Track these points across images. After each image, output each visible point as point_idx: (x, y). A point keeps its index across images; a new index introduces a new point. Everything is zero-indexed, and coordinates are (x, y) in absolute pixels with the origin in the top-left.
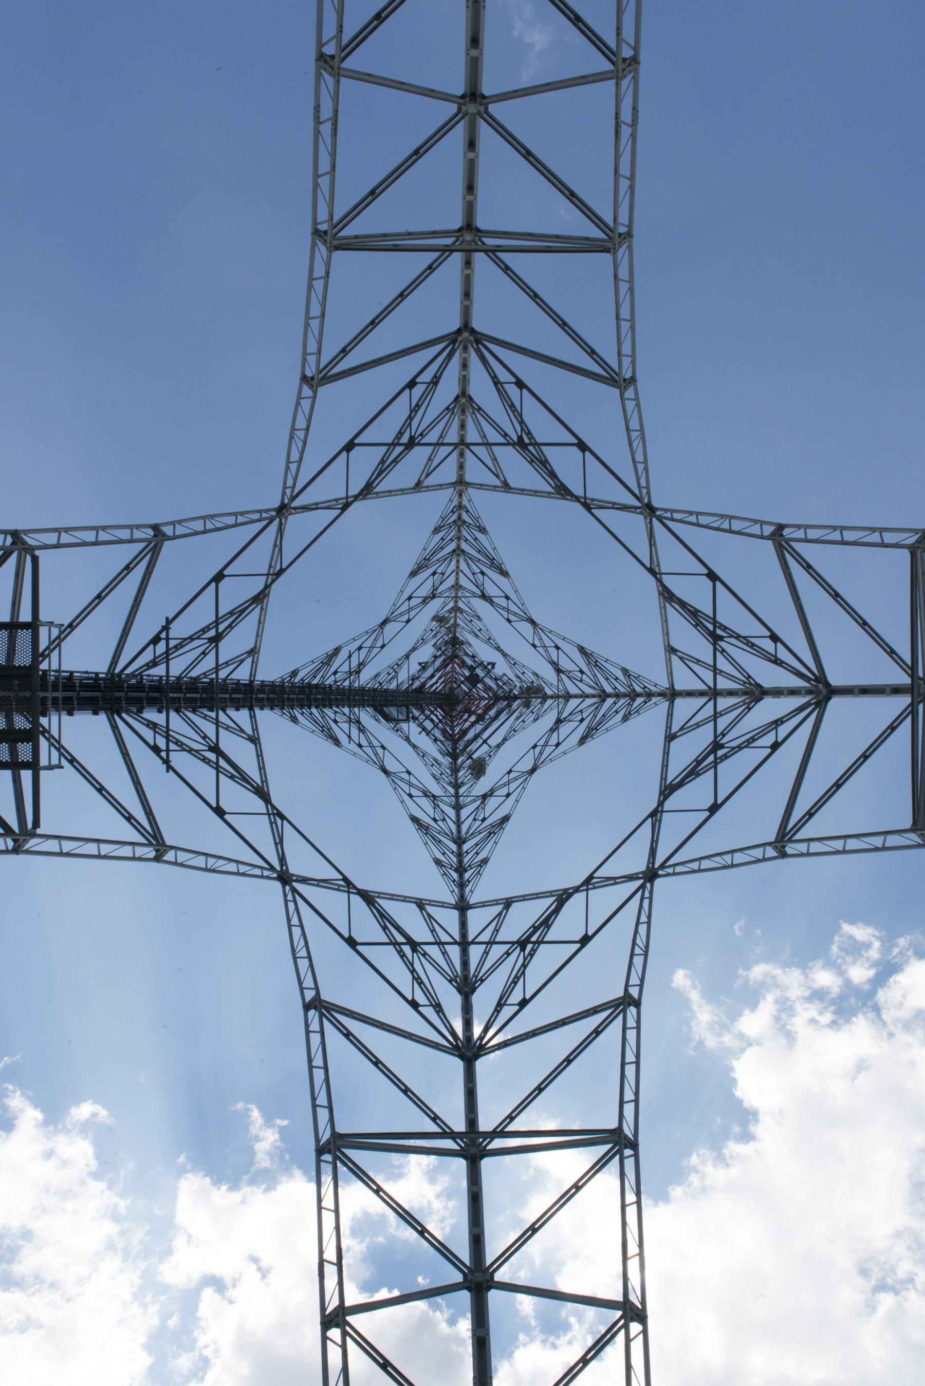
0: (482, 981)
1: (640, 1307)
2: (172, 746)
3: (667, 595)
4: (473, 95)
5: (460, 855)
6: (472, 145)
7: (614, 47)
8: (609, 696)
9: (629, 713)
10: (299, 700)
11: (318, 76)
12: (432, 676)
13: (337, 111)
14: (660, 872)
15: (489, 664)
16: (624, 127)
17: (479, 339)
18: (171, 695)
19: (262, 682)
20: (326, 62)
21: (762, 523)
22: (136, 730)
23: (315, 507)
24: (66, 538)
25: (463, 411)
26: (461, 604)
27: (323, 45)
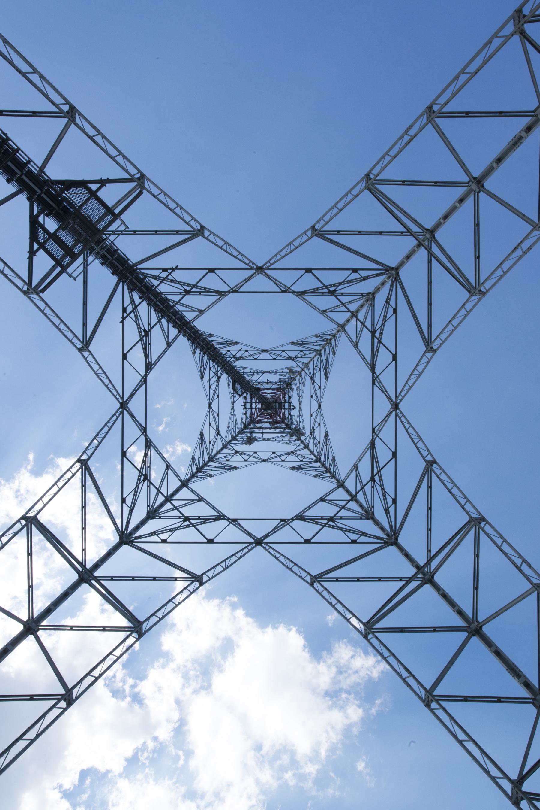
0: (160, 518)
1: (74, 698)
2: (132, 315)
4: (479, 182)
5: (205, 464)
6: (461, 201)
8: (320, 462)
9: (319, 476)
10: (202, 346)
11: (422, 115)
12: (268, 389)
13: (416, 135)
14: (263, 545)
15: (293, 406)
18: (151, 296)
19: (194, 326)
20: (430, 112)
21: (430, 453)
23: (275, 281)
24: (162, 197)
25: (367, 300)
26: (303, 373)
27: (435, 104)
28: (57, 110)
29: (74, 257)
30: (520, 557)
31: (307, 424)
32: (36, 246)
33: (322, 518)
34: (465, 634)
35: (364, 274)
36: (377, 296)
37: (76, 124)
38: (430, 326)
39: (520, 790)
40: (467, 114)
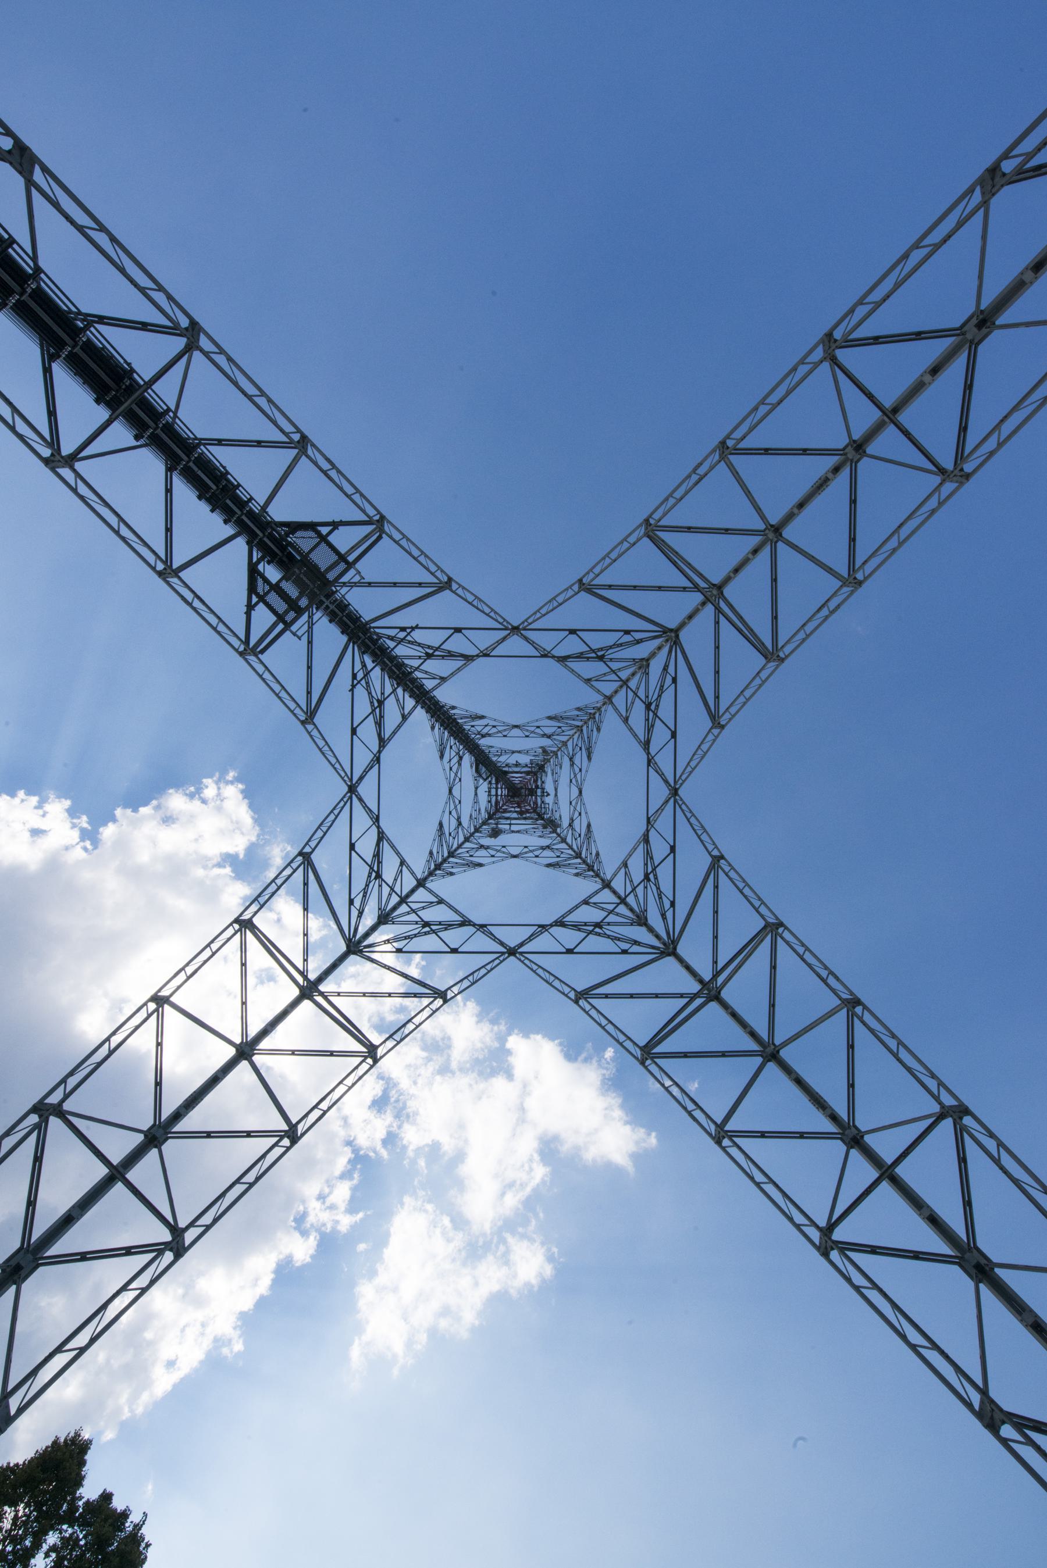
2: (363, 682)
3: (646, 839)
4: (777, 530)
5: (445, 860)
6: (755, 552)
7: (857, 567)
8: (581, 858)
11: (713, 451)
16: (826, 610)
17: (676, 642)
22: (354, 660)
24: (404, 543)
26: (559, 753)
28: (286, 439)
29: (300, 612)
30: (826, 968)
31: (564, 814)
32: (255, 599)
33: (586, 924)
34: (759, 1060)
35: (638, 636)
36: (652, 663)
37: (308, 457)
38: (717, 697)
39: (830, 1239)
40: (767, 451)
